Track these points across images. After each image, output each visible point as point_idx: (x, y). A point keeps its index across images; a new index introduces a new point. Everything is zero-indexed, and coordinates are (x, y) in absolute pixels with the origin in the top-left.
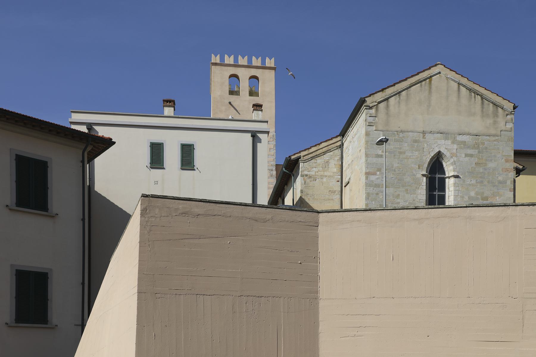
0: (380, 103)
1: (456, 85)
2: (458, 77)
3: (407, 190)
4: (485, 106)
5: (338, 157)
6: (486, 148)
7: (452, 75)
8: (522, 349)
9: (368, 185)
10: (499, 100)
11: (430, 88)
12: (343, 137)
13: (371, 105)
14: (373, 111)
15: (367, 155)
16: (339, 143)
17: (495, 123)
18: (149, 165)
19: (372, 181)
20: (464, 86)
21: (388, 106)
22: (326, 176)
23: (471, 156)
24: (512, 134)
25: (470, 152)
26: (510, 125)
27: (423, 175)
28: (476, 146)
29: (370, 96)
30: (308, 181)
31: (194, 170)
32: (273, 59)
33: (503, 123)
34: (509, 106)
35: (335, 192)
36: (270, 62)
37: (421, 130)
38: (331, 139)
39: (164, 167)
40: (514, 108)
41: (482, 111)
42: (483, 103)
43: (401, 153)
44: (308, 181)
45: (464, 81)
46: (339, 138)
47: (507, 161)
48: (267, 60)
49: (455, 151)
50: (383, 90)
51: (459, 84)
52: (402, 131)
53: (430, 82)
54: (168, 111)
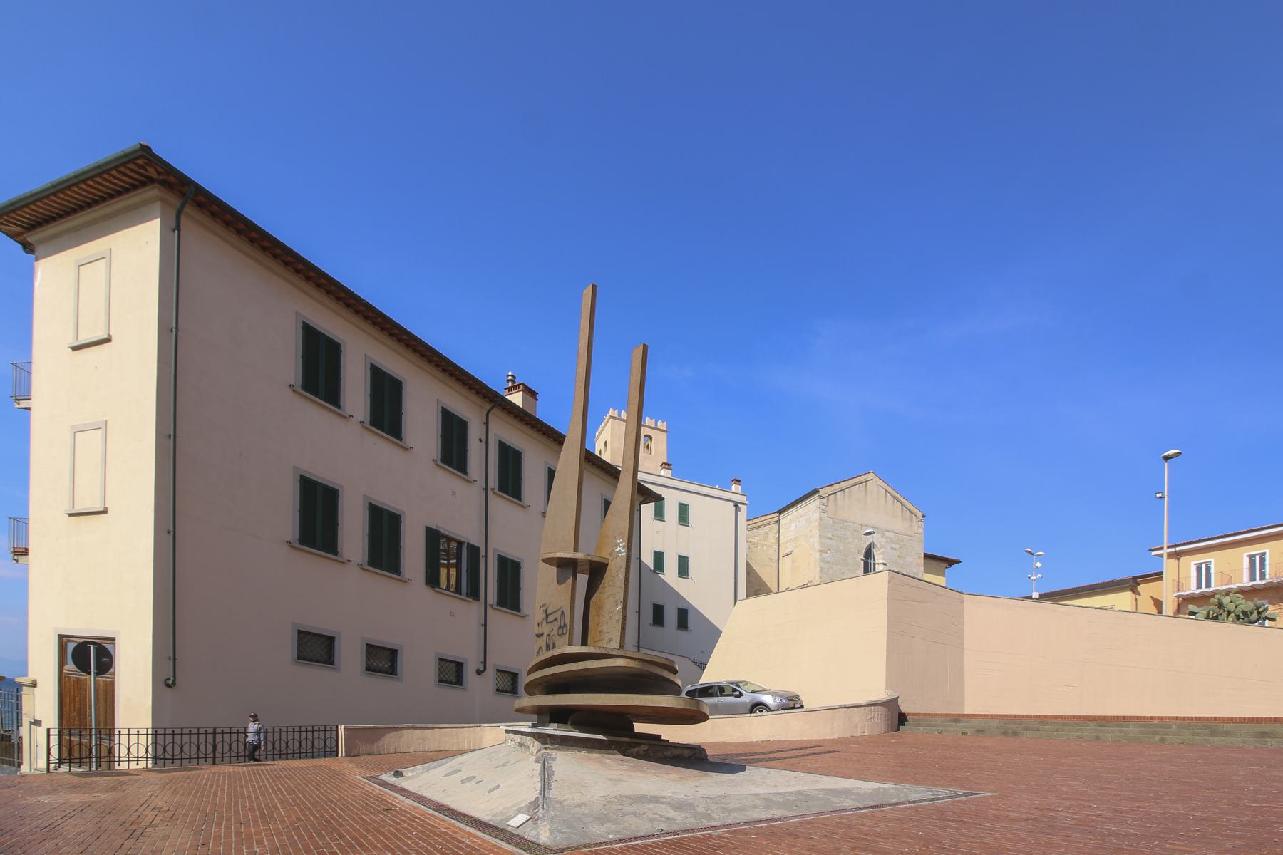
0: (830, 495)
1: (884, 491)
2: (885, 486)
3: (849, 569)
4: (904, 511)
5: (776, 530)
6: (905, 545)
7: (880, 482)
8: (394, 831)
9: (822, 560)
10: (913, 508)
11: (866, 490)
12: (780, 514)
13: (823, 496)
14: (825, 501)
15: (820, 536)
16: (776, 519)
17: (911, 526)
18: (653, 517)
19: (824, 558)
20: (889, 493)
21: (836, 499)
22: (766, 545)
23: (895, 549)
24: (922, 537)
25: (894, 546)
26: (921, 530)
27: (862, 559)
28: (898, 542)
29: (822, 488)
30: (752, 547)
31: (688, 526)
32: (665, 423)
33: (916, 528)
34: (920, 515)
35: (773, 560)
36: (661, 425)
37: (859, 523)
38: (770, 514)
39: (665, 519)
40: (923, 517)
41: (902, 515)
42: (902, 509)
43: (845, 539)
44: (752, 547)
45: (889, 489)
46: (776, 514)
47: (919, 557)
48: (659, 422)
49: (883, 543)
50: (832, 485)
51: (886, 491)
52: (846, 521)
53: (866, 485)
54: (734, 488)
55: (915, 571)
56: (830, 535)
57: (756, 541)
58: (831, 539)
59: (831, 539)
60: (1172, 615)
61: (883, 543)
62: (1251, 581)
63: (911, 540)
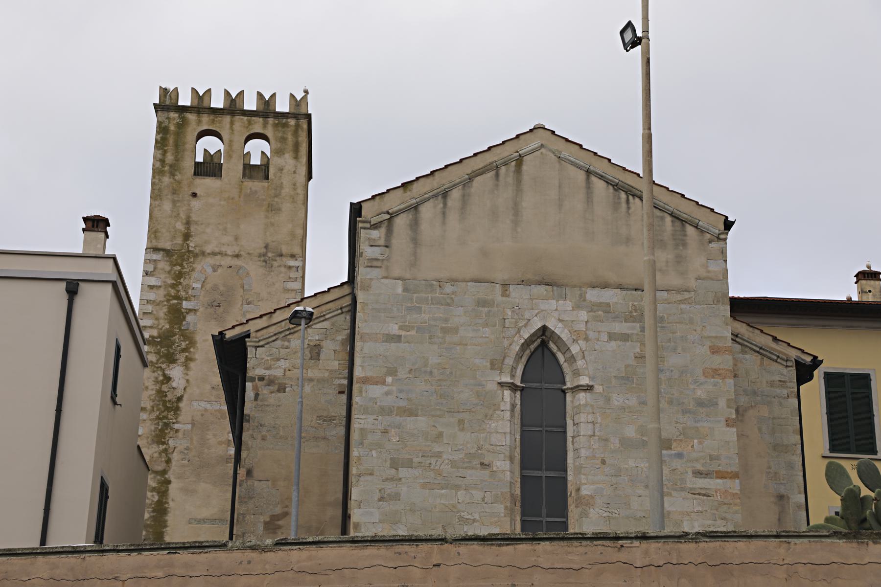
1: (581, 176)
20: (601, 177)
22: (311, 380)
23: (625, 338)
25: (620, 327)
28: (635, 316)
49: (582, 327)
51: (589, 172)
55: (700, 393)
56: (394, 329)
57: (278, 373)
58: (398, 339)
59: (398, 339)
60: (226, 332)
61: (582, 327)
62: (342, 535)
63: (681, 302)
